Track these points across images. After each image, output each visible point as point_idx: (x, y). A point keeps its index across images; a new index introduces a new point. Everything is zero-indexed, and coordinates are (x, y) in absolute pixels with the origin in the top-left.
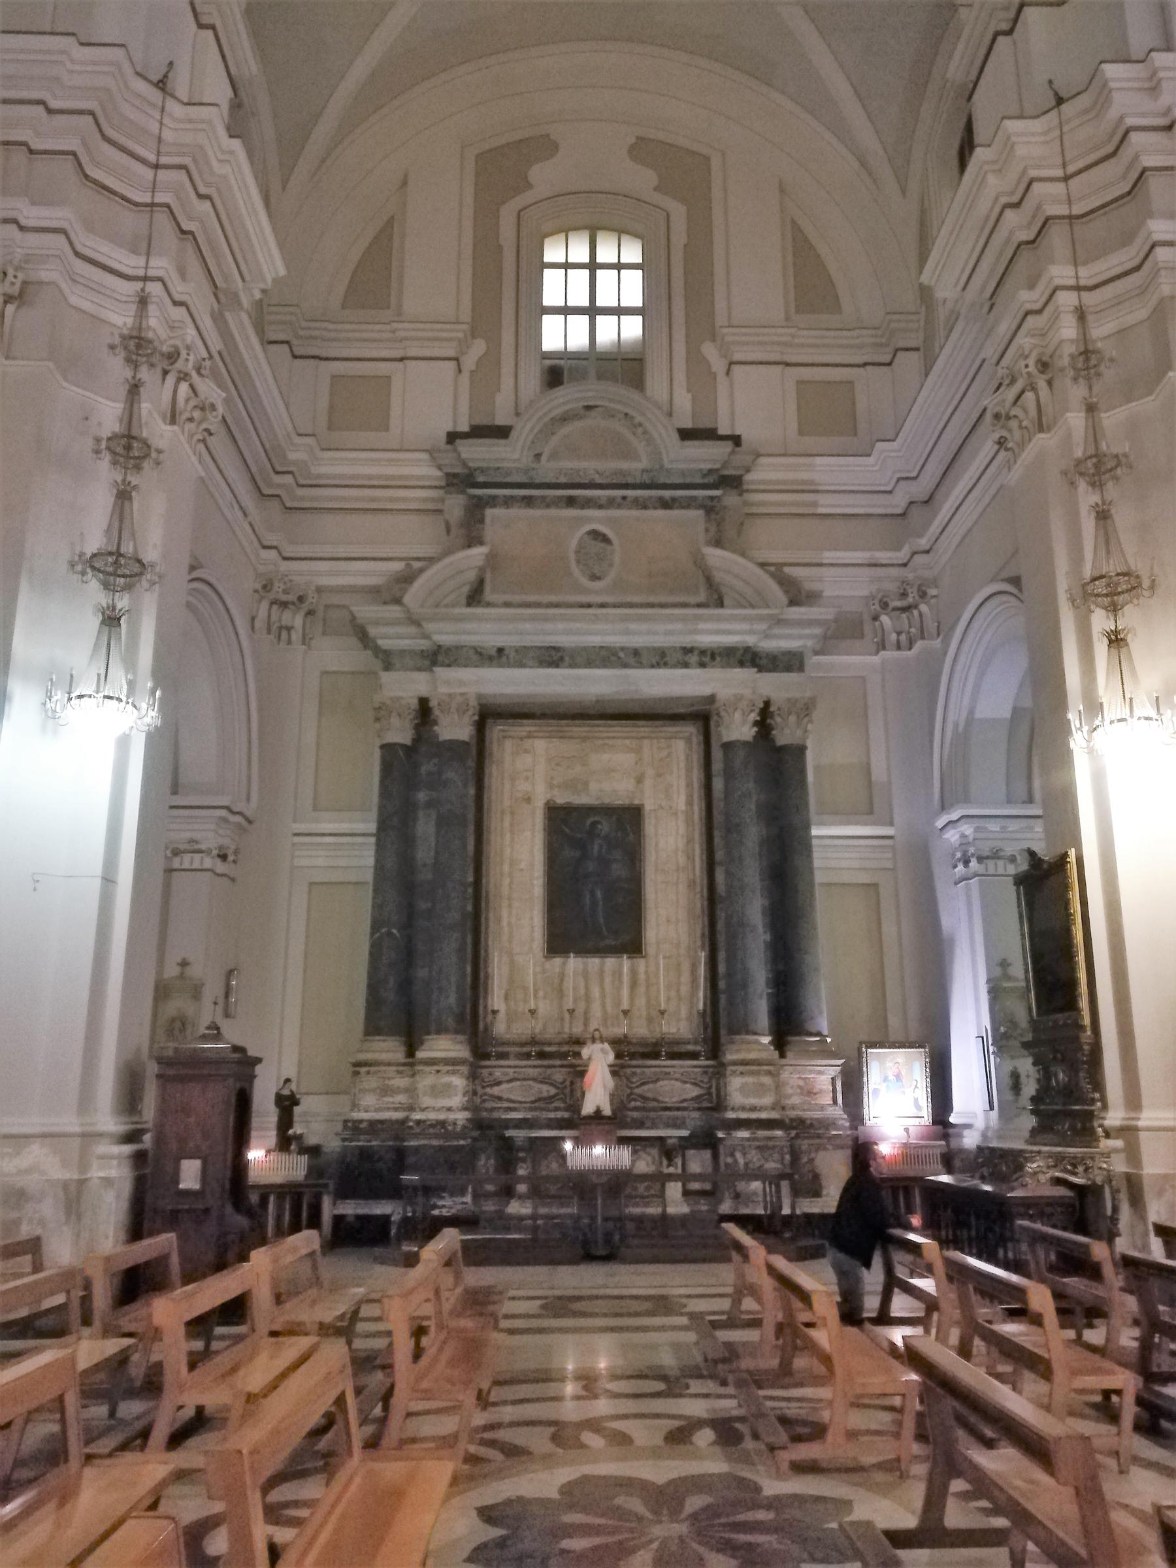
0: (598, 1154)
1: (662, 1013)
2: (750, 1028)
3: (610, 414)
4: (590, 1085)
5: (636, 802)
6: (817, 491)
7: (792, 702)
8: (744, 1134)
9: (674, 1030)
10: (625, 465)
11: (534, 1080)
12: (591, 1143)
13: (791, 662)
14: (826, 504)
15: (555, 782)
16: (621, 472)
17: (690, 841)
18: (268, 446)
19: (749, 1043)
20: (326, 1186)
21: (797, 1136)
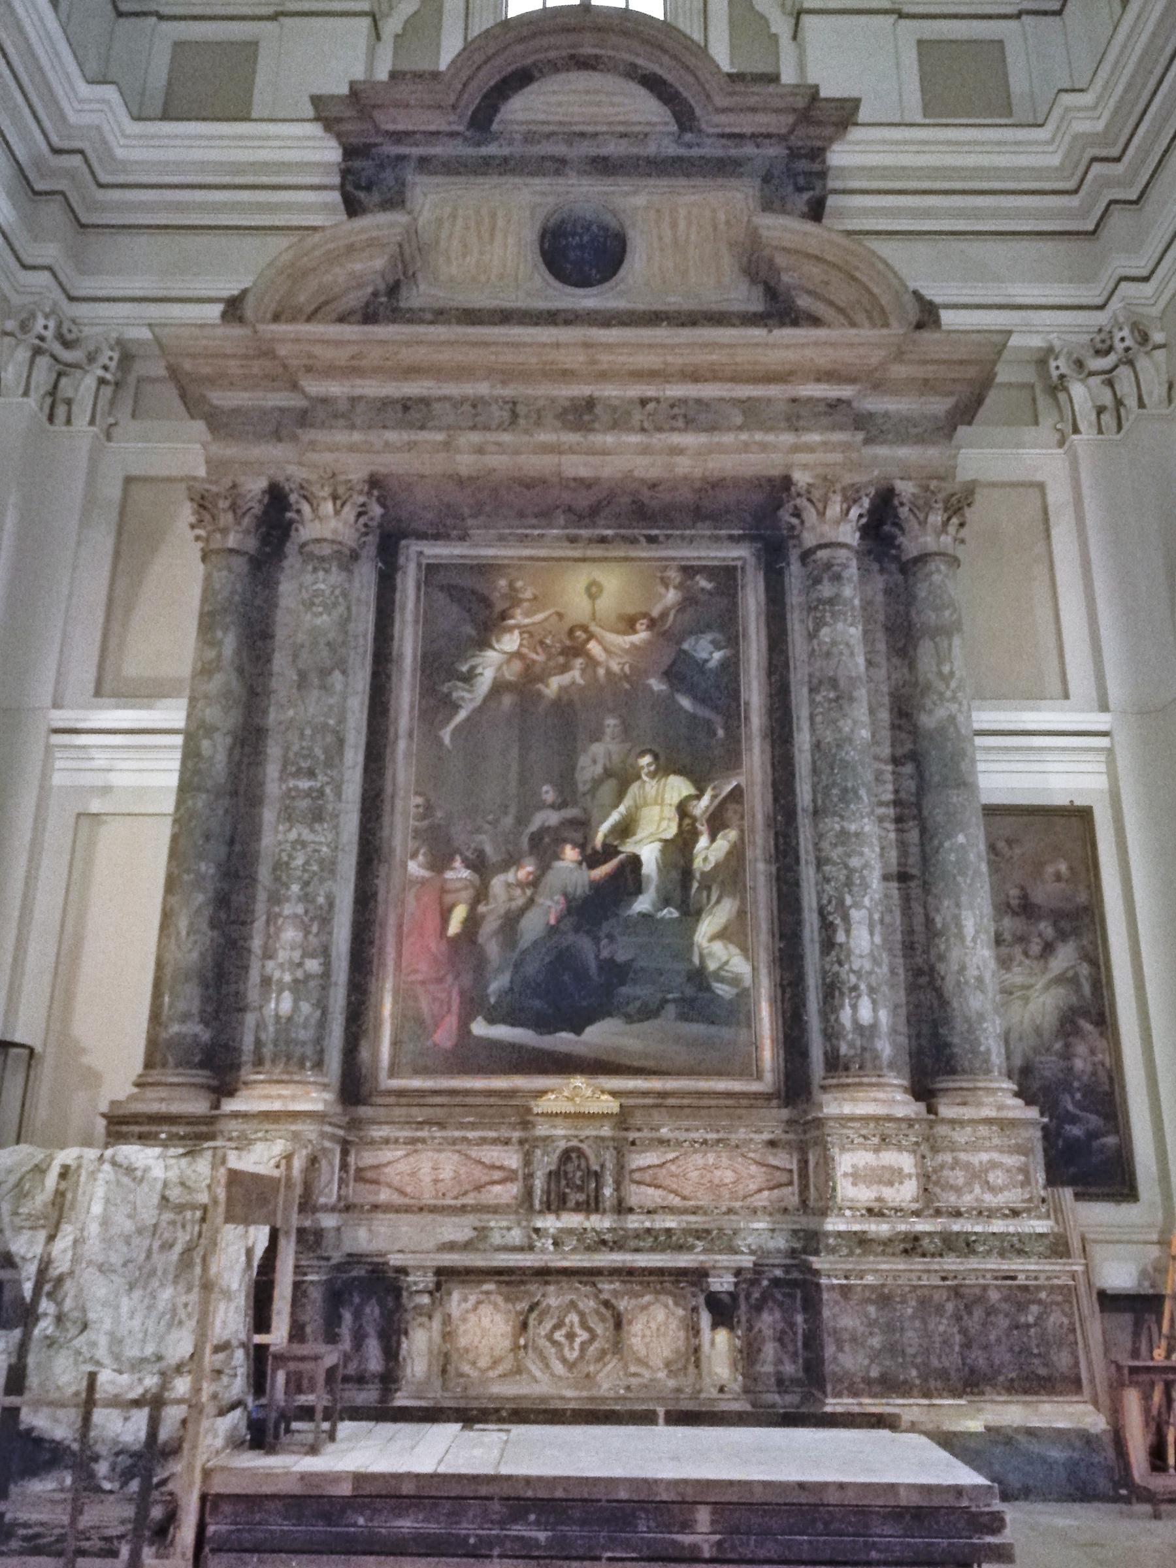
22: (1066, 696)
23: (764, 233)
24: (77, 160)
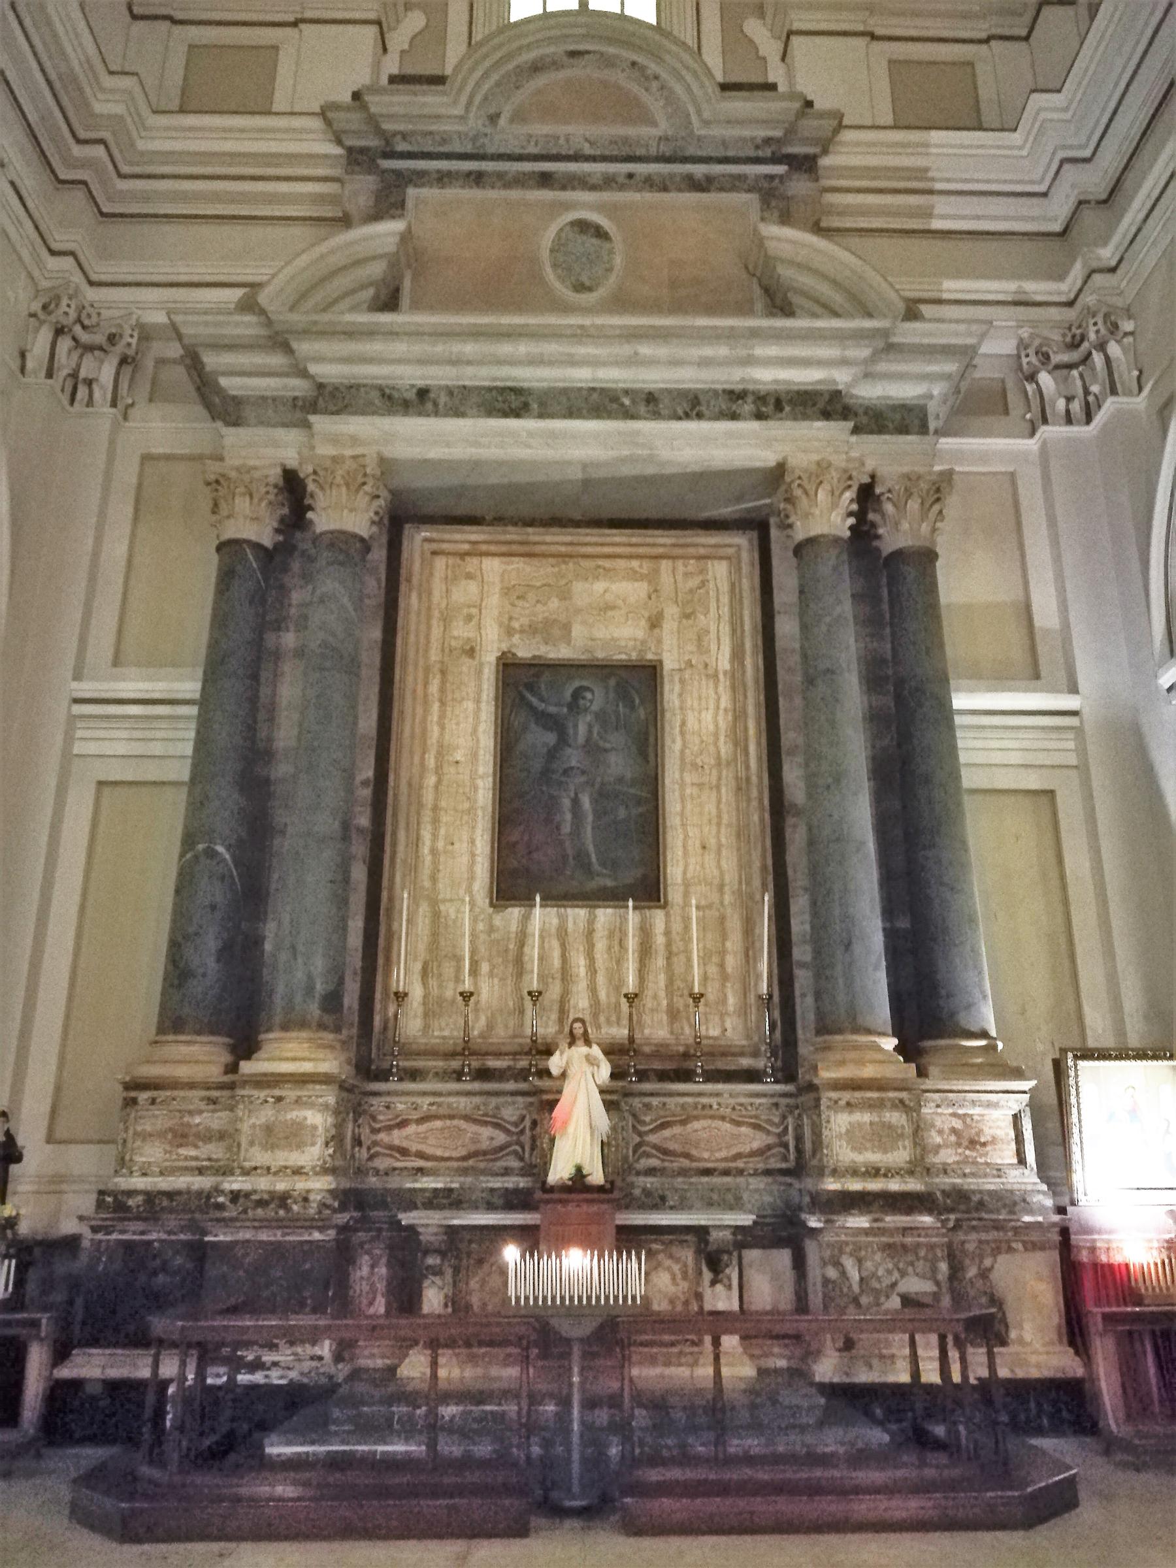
0: (577, 1266)
1: (697, 998)
2: (860, 1021)
3: (609, 62)
4: (565, 1124)
5: (650, 656)
6: (931, 192)
7: (911, 479)
8: (859, 1221)
9: (715, 1032)
10: (631, 131)
11: (467, 1118)
12: (560, 1243)
13: (906, 420)
14: (948, 215)
15: (516, 625)
16: (626, 140)
17: (739, 716)
18: (53, 76)
19: (856, 1047)
20: (35, 1324)
21: (957, 1227)
22: (1037, 676)
23: (771, 246)
24: (100, 151)
